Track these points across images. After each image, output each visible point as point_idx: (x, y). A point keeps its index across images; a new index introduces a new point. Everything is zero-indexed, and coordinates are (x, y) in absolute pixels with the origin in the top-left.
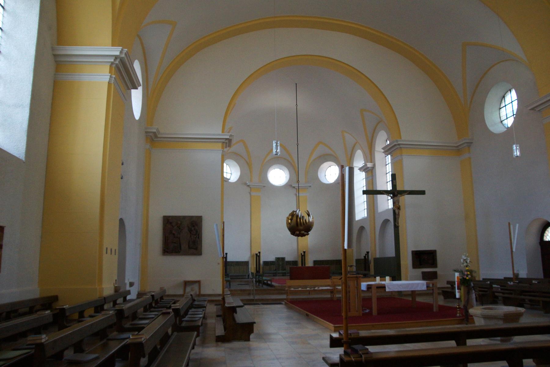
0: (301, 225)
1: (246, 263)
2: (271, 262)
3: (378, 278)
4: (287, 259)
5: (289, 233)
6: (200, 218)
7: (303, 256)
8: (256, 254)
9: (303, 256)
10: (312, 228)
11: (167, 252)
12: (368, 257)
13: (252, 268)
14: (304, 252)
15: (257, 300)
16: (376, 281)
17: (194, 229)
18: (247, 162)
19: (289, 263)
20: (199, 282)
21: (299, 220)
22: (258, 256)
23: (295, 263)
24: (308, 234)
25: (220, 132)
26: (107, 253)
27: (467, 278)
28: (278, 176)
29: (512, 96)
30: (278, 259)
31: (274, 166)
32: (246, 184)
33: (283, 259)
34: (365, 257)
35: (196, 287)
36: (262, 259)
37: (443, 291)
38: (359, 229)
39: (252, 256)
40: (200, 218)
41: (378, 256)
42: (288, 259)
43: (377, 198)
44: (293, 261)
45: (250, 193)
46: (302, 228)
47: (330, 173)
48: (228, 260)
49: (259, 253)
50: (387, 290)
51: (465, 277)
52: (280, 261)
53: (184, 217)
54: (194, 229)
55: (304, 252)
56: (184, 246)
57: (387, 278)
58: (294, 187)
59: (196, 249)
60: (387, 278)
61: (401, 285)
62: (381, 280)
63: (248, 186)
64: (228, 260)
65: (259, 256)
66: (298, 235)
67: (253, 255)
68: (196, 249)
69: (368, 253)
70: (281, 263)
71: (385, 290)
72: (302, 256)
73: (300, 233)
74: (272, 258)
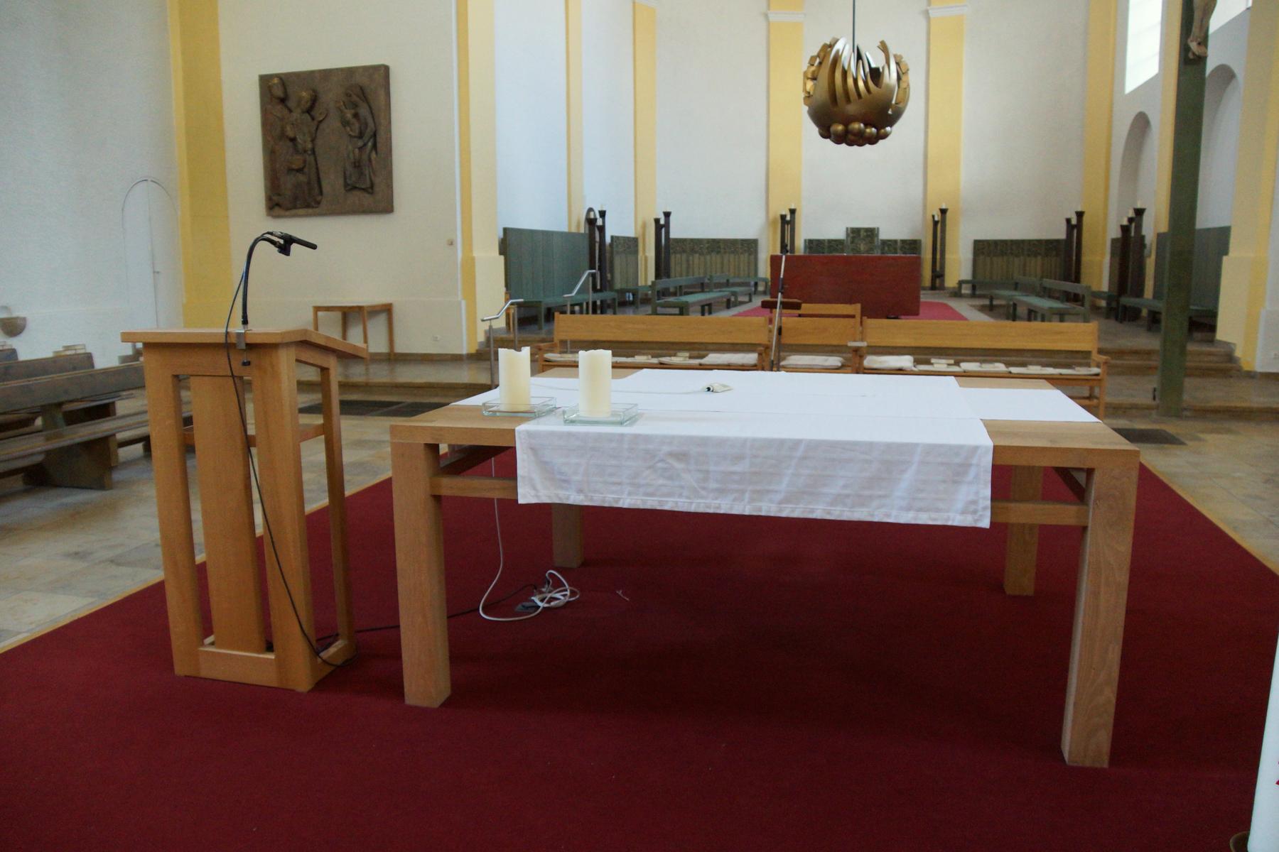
0: (848, 100)
1: (749, 247)
2: (830, 241)
4: (883, 236)
6: (381, 74)
8: (783, 217)
9: (940, 224)
11: (278, 205)
12: (1139, 227)
14: (943, 212)
17: (356, 116)
20: (387, 310)
21: (850, 81)
22: (787, 223)
24: (885, 136)
29: (1066, 755)
30: (855, 233)
33: (871, 233)
34: (1125, 229)
35: (377, 328)
36: (805, 232)
38: (1133, 126)
40: (381, 74)
42: (888, 232)
44: (903, 241)
45: (766, 16)
46: (852, 109)
48: (674, 234)
49: (793, 212)
53: (326, 74)
54: (356, 116)
55: (943, 212)
56: (332, 182)
59: (370, 189)
64: (674, 234)
65: (792, 223)
66: (839, 139)
67: (774, 222)
68: (370, 189)
69: (1139, 212)
72: (936, 223)
73: (847, 132)
74: (835, 231)
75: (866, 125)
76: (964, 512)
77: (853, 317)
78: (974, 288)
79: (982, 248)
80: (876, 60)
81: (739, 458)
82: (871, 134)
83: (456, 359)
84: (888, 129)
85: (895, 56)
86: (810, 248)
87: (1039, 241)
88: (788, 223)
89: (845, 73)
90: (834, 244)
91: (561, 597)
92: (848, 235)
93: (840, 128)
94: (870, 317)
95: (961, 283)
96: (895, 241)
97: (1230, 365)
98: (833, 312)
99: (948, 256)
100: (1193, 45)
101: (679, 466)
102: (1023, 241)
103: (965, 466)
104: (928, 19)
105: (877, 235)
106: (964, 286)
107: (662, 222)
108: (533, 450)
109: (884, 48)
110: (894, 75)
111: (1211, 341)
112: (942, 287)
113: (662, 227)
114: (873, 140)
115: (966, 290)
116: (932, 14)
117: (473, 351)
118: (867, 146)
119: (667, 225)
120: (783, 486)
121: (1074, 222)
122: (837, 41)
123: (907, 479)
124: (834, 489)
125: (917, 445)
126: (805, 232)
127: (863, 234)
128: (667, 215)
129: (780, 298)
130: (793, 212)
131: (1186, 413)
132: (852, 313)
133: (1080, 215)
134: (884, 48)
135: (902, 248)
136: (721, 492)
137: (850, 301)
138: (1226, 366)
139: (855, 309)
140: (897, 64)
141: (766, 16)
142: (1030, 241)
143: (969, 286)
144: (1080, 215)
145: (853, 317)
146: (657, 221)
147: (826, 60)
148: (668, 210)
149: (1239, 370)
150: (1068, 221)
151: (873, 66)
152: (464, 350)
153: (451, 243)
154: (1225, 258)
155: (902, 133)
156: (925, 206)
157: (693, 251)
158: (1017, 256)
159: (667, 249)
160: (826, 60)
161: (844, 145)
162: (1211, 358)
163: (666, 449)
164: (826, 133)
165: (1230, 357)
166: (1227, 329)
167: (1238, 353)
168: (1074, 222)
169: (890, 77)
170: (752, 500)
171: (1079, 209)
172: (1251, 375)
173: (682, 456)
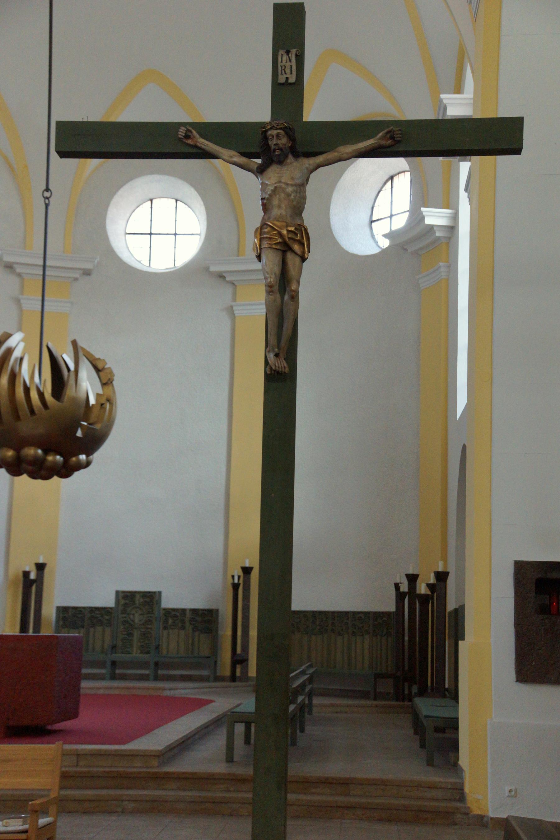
0: (18, 418)
2: (93, 610)
8: (26, 574)
18: (11, 169)
19: (176, 616)
21: (34, 395)
30: (127, 598)
33: (151, 598)
36: (60, 594)
44: (195, 611)
46: (26, 427)
49: (41, 567)
52: (139, 604)
58: (221, 276)
70: (137, 618)
72: (236, 587)
75: (46, 452)
86: (65, 619)
87: (366, 614)
88: (33, 581)
93: (10, 453)
96: (184, 611)
97: (459, 805)
102: (347, 613)
104: (21, 310)
105: (159, 602)
114: (66, 471)
116: (238, 311)
118: (56, 479)
126: (60, 594)
127: (138, 600)
130: (41, 567)
135: (192, 620)
141: (18, 302)
142: (354, 613)
150: (397, 586)
156: (225, 563)
158: (340, 634)
162: (433, 793)
168: (404, 588)
169: (87, 386)
171: (41, 561)
172: (481, 821)
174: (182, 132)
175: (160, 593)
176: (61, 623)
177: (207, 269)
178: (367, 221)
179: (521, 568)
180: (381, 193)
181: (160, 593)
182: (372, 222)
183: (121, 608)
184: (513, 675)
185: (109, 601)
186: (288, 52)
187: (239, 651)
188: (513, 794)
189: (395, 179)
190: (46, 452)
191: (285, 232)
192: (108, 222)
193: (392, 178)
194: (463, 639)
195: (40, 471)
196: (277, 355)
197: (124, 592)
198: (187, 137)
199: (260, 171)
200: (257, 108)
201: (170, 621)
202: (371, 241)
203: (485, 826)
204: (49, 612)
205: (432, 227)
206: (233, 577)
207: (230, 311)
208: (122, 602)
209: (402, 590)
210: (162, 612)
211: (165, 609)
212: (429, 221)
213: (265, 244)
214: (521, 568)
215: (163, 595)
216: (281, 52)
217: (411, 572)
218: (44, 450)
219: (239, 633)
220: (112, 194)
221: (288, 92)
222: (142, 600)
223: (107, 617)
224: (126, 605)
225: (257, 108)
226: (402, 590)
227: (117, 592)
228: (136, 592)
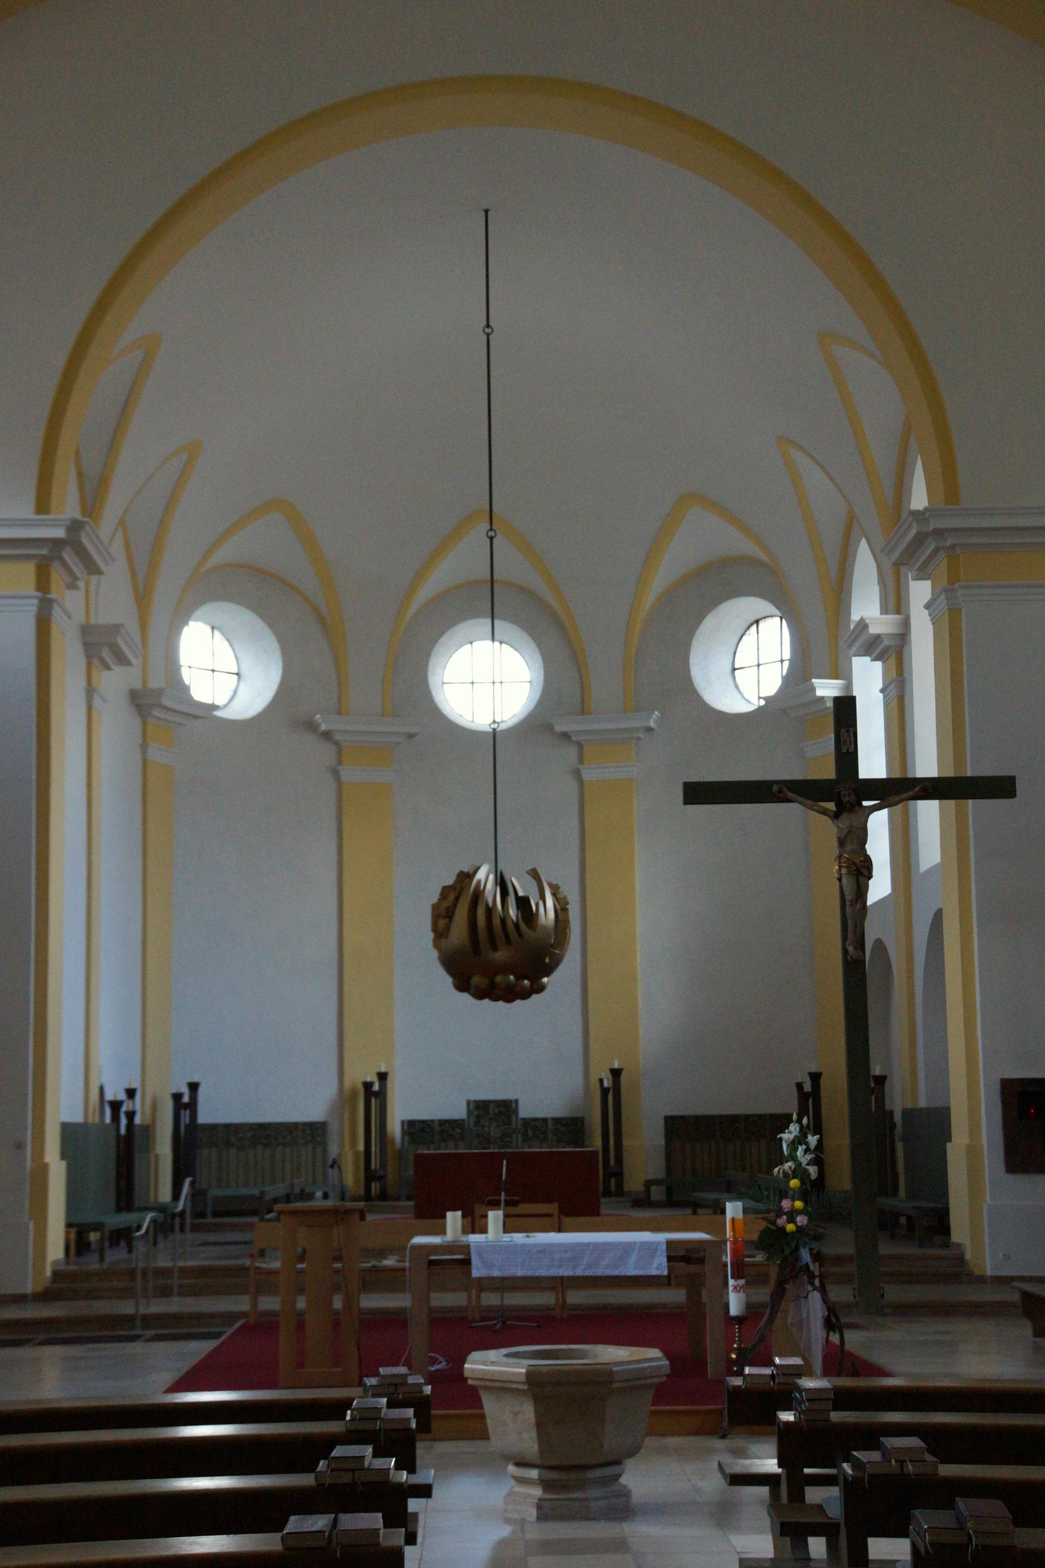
1: (313, 1133)
2: (443, 1123)
3: (453, 1219)
4: (525, 1111)
5: (448, 980)
7: (613, 1092)
8: (368, 1086)
10: (556, 963)
13: (346, 1149)
14: (616, 1073)
15: (148, 1321)
16: (442, 1231)
18: (322, 620)
19: (536, 1127)
21: (497, 921)
22: (375, 1094)
23: (571, 1127)
24: (541, 989)
25: (25, 509)
26: (938, 915)
27: (790, 1227)
28: (487, 681)
30: (480, 1108)
31: (439, 648)
32: (311, 726)
33: (506, 1108)
36: (401, 1110)
37: (1026, 1296)
39: (345, 1099)
41: (923, 1103)
43: (916, 807)
44: (557, 1121)
45: (336, 773)
46: (501, 955)
47: (747, 663)
48: (204, 1117)
49: (383, 1077)
50: (477, 1271)
51: (782, 1221)
55: (616, 1073)
57: (495, 1218)
58: (566, 736)
60: (495, 1218)
61: (544, 1250)
62: (465, 1232)
63: (327, 735)
64: (204, 1117)
65: (381, 1095)
67: (354, 1094)
71: (470, 1272)
72: (605, 1092)
76: (657, 1269)
77: (551, 1215)
78: (669, 1191)
79: (679, 1129)
80: (521, 886)
81: (566, 1252)
82: (523, 987)
83: (19, 1299)
84: (545, 980)
85: (551, 886)
86: (410, 1134)
88: (376, 1094)
89: (503, 921)
90: (448, 1128)
91: (512, 977)
92: (469, 1112)
94: (567, 1215)
95: (649, 1184)
96: (545, 1120)
98: (532, 1212)
99: (626, 1142)
100: (851, 949)
101: (541, 1256)
103: (656, 1250)
105: (516, 1111)
106: (653, 1188)
107: (186, 1099)
108: (479, 1253)
109: (534, 874)
110: (551, 914)
111: (947, 1244)
112: (620, 1192)
113: (185, 1104)
114: (525, 995)
115: (658, 1193)
116: (587, 775)
117: (40, 1289)
119: (193, 1105)
120: (585, 1262)
121: (808, 1087)
122: (479, 868)
123: (633, 1257)
124: (604, 1263)
125: (635, 1243)
126: (401, 1110)
128: (194, 1087)
129: (503, 1196)
130: (383, 1077)
131: (887, 1310)
132: (550, 1211)
133: (815, 1077)
134: (534, 874)
136: (560, 1266)
137: (549, 1201)
138: (957, 1271)
139: (553, 1208)
140: (554, 895)
141: (336, 773)
143: (663, 1188)
144: (815, 1077)
145: (551, 1215)
146: (799, 1086)
147: (459, 893)
148: (195, 1080)
149: (970, 1274)
150: (799, 1086)
151: (521, 894)
152: (29, 1289)
153: (20, 1146)
154: (949, 1145)
155: (561, 982)
157: (228, 1144)
159: (192, 1139)
160: (459, 893)
161: (486, 1002)
163: (536, 1249)
164: (462, 985)
165: (960, 1260)
166: (960, 1232)
167: (968, 1256)
168: (808, 1087)
169: (547, 912)
170: (573, 1269)
171: (383, 1070)
173: (543, 1252)
174: (775, 788)
175: (517, 1101)
176: (406, 1138)
177: (549, 728)
178: (729, 668)
179: (1007, 1085)
180: (744, 638)
181: (517, 1101)
182: (734, 669)
183: (472, 1120)
184: (1002, 1166)
185: (459, 1112)
186: (848, 731)
187: (612, 1162)
188: (1007, 1257)
189: (761, 624)
190: (519, 977)
191: (858, 862)
192: (430, 674)
193: (757, 622)
194: (950, 1141)
195: (510, 995)
196: (855, 948)
197: (475, 1102)
198: (780, 792)
199: (836, 816)
200: (828, 771)
201: (530, 1133)
202: (736, 692)
203: (985, 1282)
204: (395, 1129)
205: (822, 698)
206: (601, 1081)
207: (577, 774)
208: (476, 1113)
209: (806, 1090)
210: (519, 1124)
211: (523, 1119)
212: (819, 693)
213: (844, 871)
214: (1007, 1085)
215: (520, 1102)
216: (843, 730)
217: (814, 1070)
218: (516, 977)
219: (612, 1142)
220: (434, 641)
221: (900, 790)
222: (497, 1111)
223: (458, 1131)
224: (478, 1117)
225: (828, 771)
226: (806, 1090)
227: (468, 1102)
228: (490, 1101)
